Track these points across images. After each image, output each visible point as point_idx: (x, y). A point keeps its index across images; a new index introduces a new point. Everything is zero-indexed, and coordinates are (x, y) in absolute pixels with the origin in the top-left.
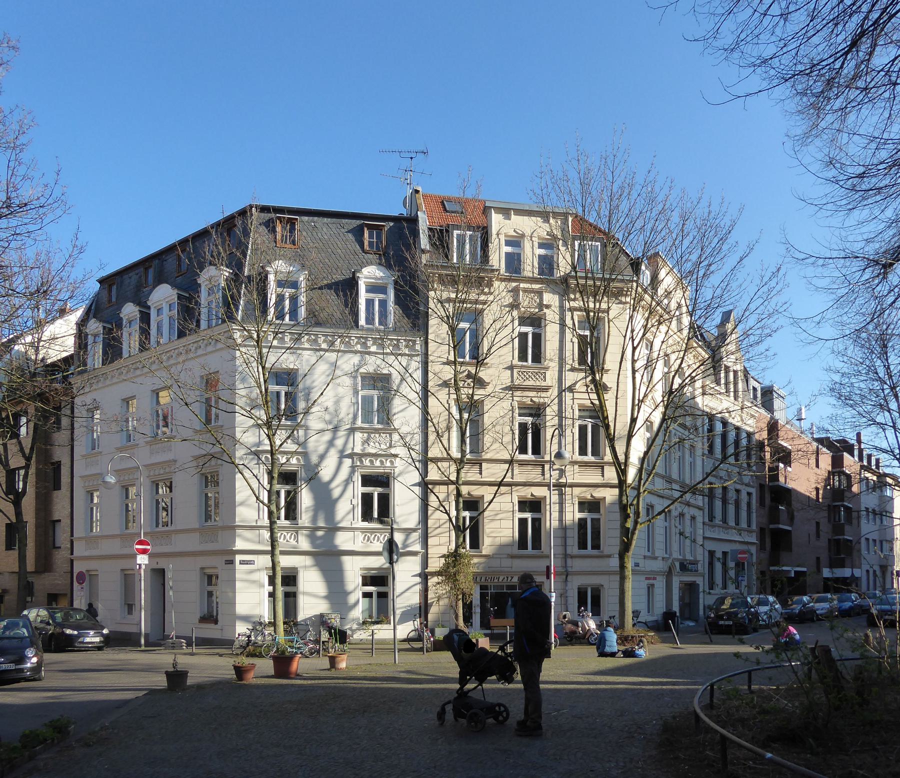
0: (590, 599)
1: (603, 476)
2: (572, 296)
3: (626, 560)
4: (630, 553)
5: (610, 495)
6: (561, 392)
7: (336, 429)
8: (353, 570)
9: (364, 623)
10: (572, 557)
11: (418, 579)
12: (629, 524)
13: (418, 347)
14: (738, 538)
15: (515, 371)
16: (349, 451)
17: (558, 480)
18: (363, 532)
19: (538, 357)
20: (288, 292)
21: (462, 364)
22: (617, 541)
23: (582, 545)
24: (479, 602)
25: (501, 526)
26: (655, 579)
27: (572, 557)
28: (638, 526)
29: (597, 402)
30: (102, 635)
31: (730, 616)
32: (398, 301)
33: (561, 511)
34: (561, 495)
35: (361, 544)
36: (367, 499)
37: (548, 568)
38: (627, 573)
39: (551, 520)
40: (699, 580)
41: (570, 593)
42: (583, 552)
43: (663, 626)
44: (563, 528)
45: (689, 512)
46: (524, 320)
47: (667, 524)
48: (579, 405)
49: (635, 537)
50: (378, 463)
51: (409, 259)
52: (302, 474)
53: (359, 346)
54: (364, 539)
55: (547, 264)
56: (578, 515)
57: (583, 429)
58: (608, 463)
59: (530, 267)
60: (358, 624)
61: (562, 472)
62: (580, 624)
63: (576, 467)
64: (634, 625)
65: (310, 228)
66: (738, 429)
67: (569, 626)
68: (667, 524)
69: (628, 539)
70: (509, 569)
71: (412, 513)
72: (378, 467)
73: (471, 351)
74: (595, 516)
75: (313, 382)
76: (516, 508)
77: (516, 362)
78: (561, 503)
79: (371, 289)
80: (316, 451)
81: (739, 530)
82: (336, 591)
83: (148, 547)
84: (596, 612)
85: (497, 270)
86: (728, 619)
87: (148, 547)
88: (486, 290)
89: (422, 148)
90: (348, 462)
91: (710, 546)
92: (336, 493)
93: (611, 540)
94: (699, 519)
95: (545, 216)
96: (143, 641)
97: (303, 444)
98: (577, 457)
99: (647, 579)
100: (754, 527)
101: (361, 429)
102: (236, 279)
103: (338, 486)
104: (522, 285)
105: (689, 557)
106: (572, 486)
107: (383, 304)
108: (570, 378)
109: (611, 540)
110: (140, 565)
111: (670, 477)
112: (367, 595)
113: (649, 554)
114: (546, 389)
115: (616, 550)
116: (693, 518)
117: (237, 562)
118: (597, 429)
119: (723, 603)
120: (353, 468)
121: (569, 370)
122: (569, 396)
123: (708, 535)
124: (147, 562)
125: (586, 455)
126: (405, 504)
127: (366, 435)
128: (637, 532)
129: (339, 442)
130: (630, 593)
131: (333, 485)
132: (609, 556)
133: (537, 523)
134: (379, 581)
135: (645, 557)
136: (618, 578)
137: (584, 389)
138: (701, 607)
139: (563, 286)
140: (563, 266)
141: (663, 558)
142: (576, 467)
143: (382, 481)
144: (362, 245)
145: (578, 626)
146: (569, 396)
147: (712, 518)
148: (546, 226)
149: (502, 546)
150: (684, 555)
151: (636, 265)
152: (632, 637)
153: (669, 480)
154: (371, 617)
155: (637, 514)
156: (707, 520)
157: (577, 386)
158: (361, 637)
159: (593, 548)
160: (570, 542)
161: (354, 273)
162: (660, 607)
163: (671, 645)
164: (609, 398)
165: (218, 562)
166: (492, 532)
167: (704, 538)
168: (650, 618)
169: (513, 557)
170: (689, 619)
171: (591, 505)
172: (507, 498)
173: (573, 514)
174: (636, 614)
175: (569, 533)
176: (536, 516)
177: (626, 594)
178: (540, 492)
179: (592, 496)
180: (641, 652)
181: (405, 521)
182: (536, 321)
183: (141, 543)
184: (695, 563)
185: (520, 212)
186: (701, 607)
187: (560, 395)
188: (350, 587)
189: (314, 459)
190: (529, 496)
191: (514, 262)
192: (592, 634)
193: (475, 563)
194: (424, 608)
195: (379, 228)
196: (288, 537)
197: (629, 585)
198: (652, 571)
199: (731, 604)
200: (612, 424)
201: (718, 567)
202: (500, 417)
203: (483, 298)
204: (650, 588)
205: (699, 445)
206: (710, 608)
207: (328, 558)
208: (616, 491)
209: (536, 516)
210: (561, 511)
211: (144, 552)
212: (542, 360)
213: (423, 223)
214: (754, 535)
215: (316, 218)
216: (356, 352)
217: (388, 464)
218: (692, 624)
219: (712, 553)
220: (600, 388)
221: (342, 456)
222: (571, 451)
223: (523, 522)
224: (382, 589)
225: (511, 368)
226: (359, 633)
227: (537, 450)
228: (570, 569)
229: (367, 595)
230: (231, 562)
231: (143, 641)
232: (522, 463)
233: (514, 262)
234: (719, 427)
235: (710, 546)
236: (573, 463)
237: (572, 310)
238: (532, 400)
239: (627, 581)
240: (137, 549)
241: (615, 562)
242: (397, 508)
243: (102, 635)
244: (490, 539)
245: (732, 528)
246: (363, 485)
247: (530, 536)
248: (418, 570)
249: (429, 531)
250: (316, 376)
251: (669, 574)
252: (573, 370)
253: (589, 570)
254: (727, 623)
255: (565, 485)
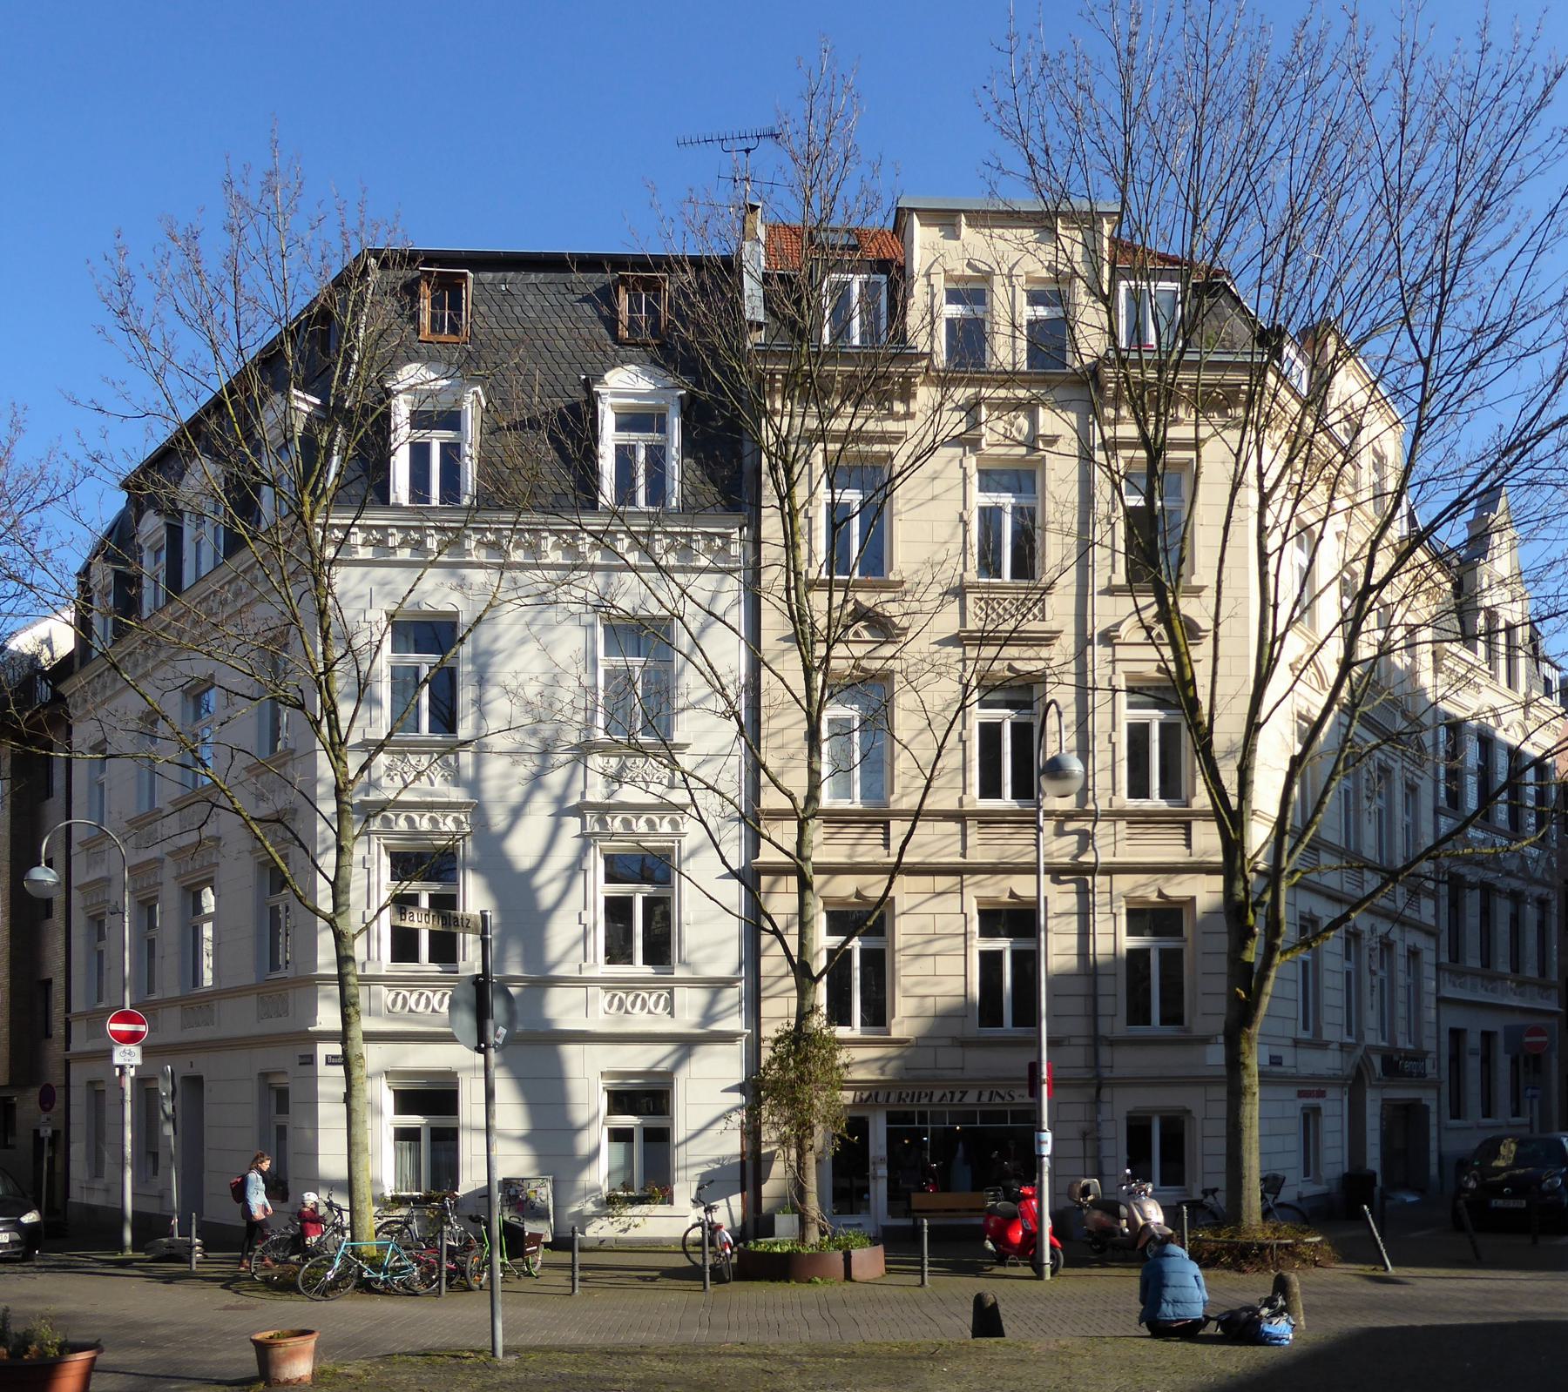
0: (1158, 1148)
1: (1189, 846)
2: (1109, 412)
3: (1244, 1046)
4: (1255, 1030)
5: (1206, 892)
6: (1083, 642)
7: (546, 752)
8: (588, 1077)
9: (611, 1201)
10: (1113, 1043)
11: (737, 1099)
12: (1252, 954)
13: (735, 550)
14: (1515, 1001)
15: (970, 598)
16: (574, 800)
17: (1076, 857)
18: (607, 989)
19: (1025, 564)
20: (436, 440)
21: (846, 586)
22: (1221, 1005)
23: (1138, 1013)
24: (883, 1153)
25: (938, 966)
26: (1321, 1094)
27: (1113, 1043)
28: (1277, 959)
29: (1172, 667)
30: (19, 1227)
31: (1520, 1186)
32: (688, 448)
33: (1084, 933)
34: (1084, 893)
35: (602, 1015)
36: (618, 910)
37: (1034, 1068)
38: (1246, 1081)
39: (1058, 950)
40: (1428, 1097)
41: (1107, 1130)
42: (1140, 1030)
43: (1342, 1213)
44: (1088, 968)
45: (1404, 940)
46: (990, 479)
47: (1350, 966)
48: (1130, 676)
49: (1269, 987)
50: (641, 826)
51: (734, 376)
52: (468, 849)
53: (598, 554)
54: (610, 1004)
55: (1050, 342)
56: (1127, 942)
57: (1138, 734)
58: (1202, 815)
59: (1007, 350)
60: (599, 1203)
61: (1086, 839)
62: (1123, 1210)
63: (1122, 825)
64: (1266, 1214)
65: (497, 297)
66: (1515, 753)
67: (1097, 1214)
68: (1350, 966)
69: (1248, 992)
70: (958, 1074)
71: (723, 942)
72: (650, 833)
73: (863, 546)
74: (1170, 943)
75: (496, 639)
76: (975, 926)
77: (972, 576)
78: (1084, 913)
79: (629, 421)
80: (502, 799)
81: (1521, 984)
82: (551, 1130)
83: (142, 1028)
84: (1173, 1173)
85: (922, 356)
86: (1514, 1195)
87: (142, 1028)
88: (899, 407)
89: (765, 125)
90: (573, 825)
91: (1455, 1018)
92: (548, 896)
93: (1206, 1002)
94: (1428, 957)
95: (1044, 223)
96: (128, 1236)
97: (474, 786)
98: (1124, 801)
99: (1301, 1094)
100: (1554, 975)
101: (604, 750)
102: (329, 413)
103: (552, 880)
104: (986, 392)
105: (1403, 1043)
106: (1111, 870)
107: (657, 457)
108: (1107, 611)
109: (1206, 1002)
110: (122, 1068)
111: (1358, 855)
112: (618, 1135)
113: (1307, 1036)
114: (1047, 639)
115: (1217, 1025)
116: (1414, 954)
117: (321, 1060)
118: (1179, 736)
119: (1497, 1155)
120: (586, 839)
121: (1101, 593)
122: (1100, 653)
123: (1449, 992)
124: (138, 1061)
125: (1147, 796)
126: (708, 926)
127: (614, 761)
128: (1273, 974)
129: (556, 779)
130: (1256, 1133)
131: (541, 877)
132: (1205, 1041)
133: (1027, 963)
134: (644, 1100)
135: (1297, 1043)
136: (1221, 1092)
137: (1141, 636)
138: (1434, 1158)
139: (1086, 390)
140: (1090, 341)
141: (1342, 1046)
142: (1122, 825)
143: (653, 866)
144: (612, 324)
145: (1118, 1217)
146: (1100, 653)
147: (1456, 953)
148: (1047, 252)
149: (945, 1018)
150: (1393, 1039)
151: (1270, 339)
152: (1262, 1247)
153: (1352, 859)
154: (627, 1186)
155: (1273, 927)
156: (1445, 959)
157: (1123, 631)
158: (602, 1234)
159: (1164, 1021)
160: (1105, 1005)
161: (587, 386)
162: (1334, 1157)
163: (1367, 1269)
164: (1201, 653)
165: (281, 1059)
166: (917, 984)
167: (1440, 1000)
168: (1311, 1190)
169: (964, 1043)
170: (1406, 1186)
171: (1155, 918)
172: (953, 902)
173: (1114, 937)
174: (1272, 1184)
175: (1105, 985)
176: (1025, 945)
177: (1246, 1135)
178: (1024, 886)
179: (1161, 894)
180: (1280, 1327)
181: (711, 960)
182: (1022, 477)
183: (125, 1018)
184: (1418, 1056)
185: (980, 218)
186: (1434, 1158)
187: (1080, 655)
188: (580, 1115)
189: (498, 820)
190: (1005, 898)
191: (969, 339)
192: (1153, 1237)
193: (859, 1058)
194: (751, 1169)
195: (653, 286)
196: (435, 1002)
197: (1252, 1111)
198: (1313, 1076)
199: (1517, 1156)
200: (1203, 696)
201: (1473, 1065)
202: (933, 708)
203: (890, 426)
204: (1311, 1116)
205: (1426, 787)
206: (1462, 1165)
207: (534, 1054)
208: (1218, 882)
209: (1025, 945)
210: (1084, 933)
211: (132, 1038)
212: (1038, 572)
213: (755, 260)
214: (1554, 994)
215: (511, 275)
216: (593, 568)
217: (666, 827)
218: (1411, 1199)
219: (1457, 1035)
220: (1177, 631)
221: (562, 811)
222: (1109, 781)
223: (990, 962)
224: (655, 1122)
225: (959, 592)
226: (598, 1223)
227: (1025, 788)
228: (1106, 1073)
229: (618, 1135)
230: (310, 1060)
231: (128, 1236)
232: (987, 819)
233: (969, 339)
234: (1471, 753)
235: (1455, 1018)
236: (1116, 815)
237: (1111, 446)
238: (1011, 668)
239: (1248, 1099)
240: (115, 1034)
241: (1216, 1055)
242: (686, 931)
243: (19, 1227)
244: (913, 1002)
245: (1503, 978)
246: (610, 878)
247: (1008, 995)
248: (737, 1074)
249: (764, 983)
250: (500, 628)
251: (1355, 1084)
252: (1111, 591)
253: (1148, 1074)
254: (1512, 1204)
255: (1093, 870)
